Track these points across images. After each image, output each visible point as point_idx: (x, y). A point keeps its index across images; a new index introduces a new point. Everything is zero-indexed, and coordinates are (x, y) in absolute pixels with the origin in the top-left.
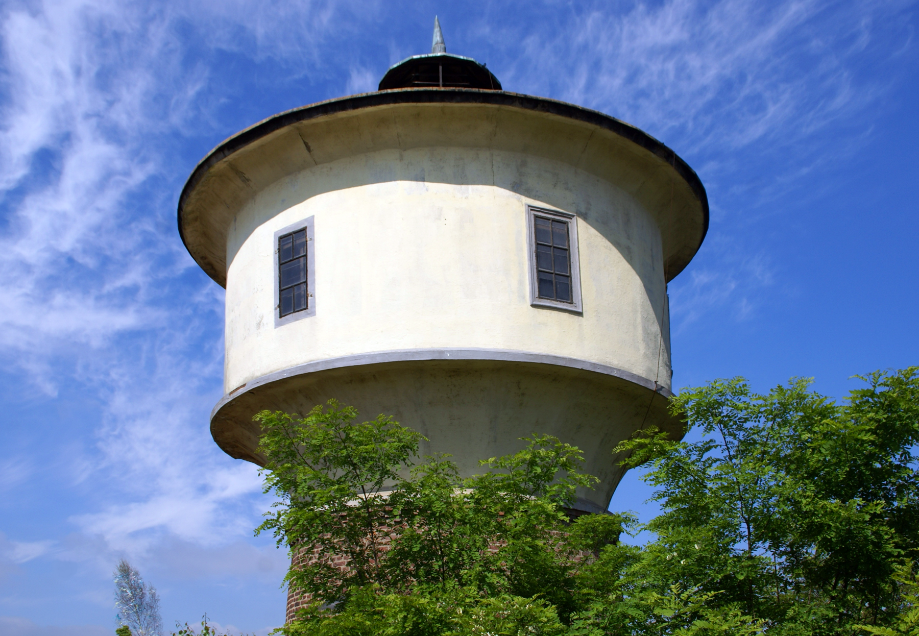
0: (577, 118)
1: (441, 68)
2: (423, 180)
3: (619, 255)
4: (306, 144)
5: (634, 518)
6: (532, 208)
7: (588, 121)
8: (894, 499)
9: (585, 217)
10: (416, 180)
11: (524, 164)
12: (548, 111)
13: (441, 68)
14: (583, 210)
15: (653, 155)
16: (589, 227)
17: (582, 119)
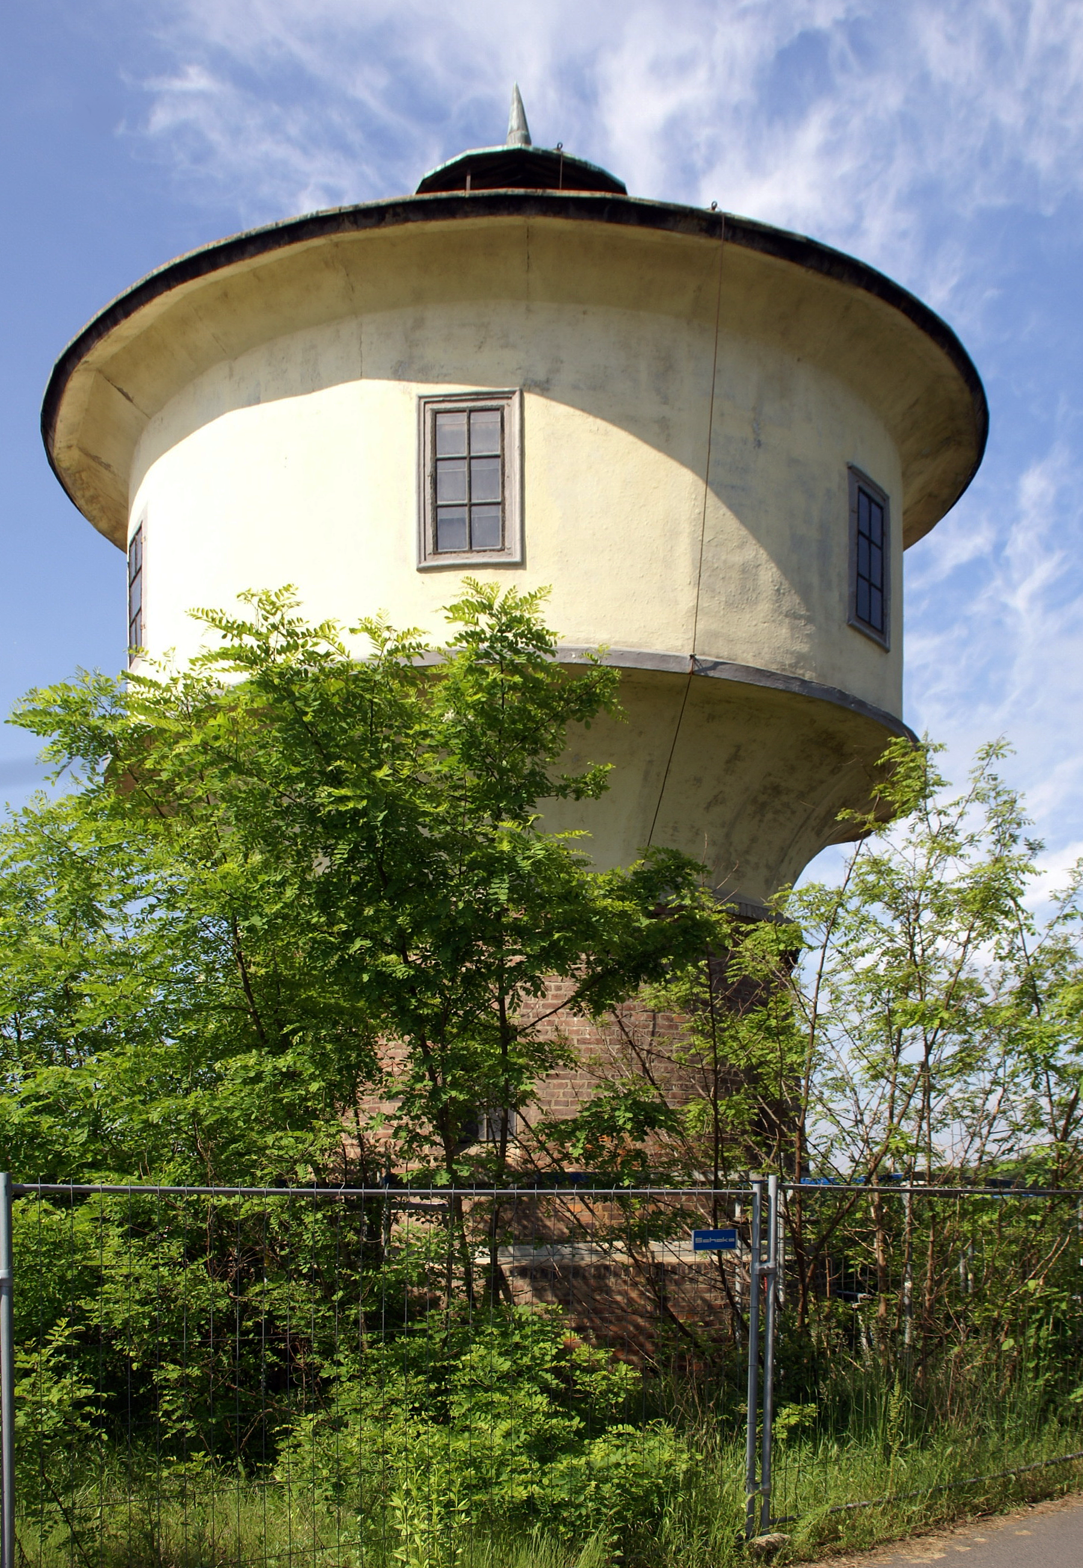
0: (466, 215)
1: (469, 178)
2: (258, 401)
3: (631, 439)
4: (120, 390)
5: (936, 742)
6: (425, 400)
7: (491, 214)
8: (29, 1503)
9: (544, 388)
10: (249, 404)
11: (419, 323)
12: (407, 220)
13: (469, 178)
14: (541, 375)
15: (676, 236)
16: (554, 404)
17: (478, 214)
